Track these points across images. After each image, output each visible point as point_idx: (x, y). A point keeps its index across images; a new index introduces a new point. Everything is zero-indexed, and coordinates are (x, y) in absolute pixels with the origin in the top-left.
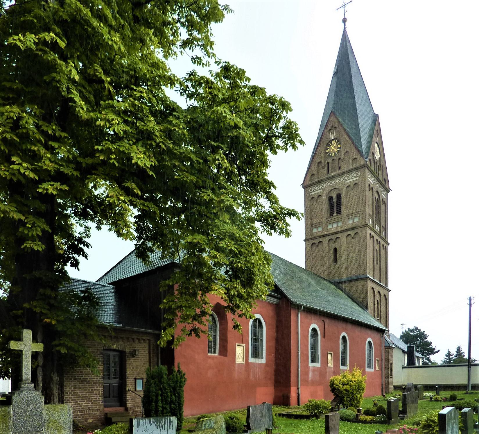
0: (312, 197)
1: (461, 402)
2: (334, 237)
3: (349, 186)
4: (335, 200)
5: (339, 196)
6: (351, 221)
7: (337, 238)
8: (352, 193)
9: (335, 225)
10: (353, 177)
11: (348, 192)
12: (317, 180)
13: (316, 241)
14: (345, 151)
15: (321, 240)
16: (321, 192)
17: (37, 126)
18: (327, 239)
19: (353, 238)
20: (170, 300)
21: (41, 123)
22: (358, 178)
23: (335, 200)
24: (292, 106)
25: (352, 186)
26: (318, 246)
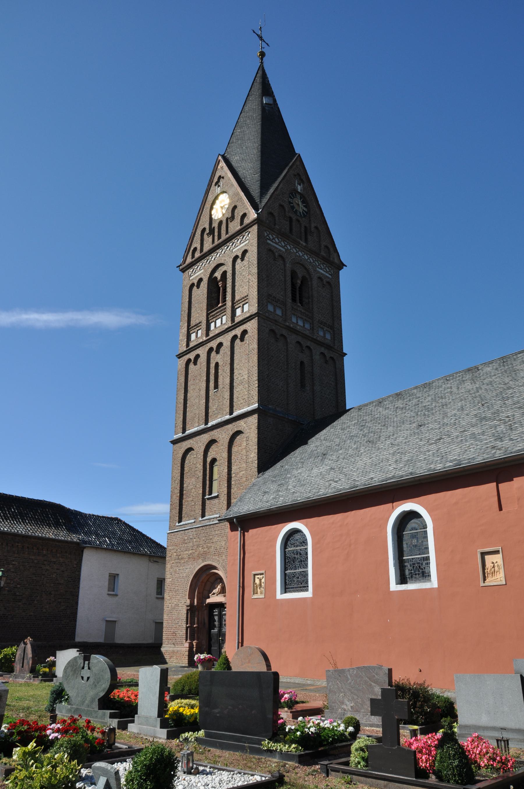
4: (299, 282)
7: (282, 335)
9: (300, 323)
10: (280, 244)
15: (285, 332)
22: (284, 250)
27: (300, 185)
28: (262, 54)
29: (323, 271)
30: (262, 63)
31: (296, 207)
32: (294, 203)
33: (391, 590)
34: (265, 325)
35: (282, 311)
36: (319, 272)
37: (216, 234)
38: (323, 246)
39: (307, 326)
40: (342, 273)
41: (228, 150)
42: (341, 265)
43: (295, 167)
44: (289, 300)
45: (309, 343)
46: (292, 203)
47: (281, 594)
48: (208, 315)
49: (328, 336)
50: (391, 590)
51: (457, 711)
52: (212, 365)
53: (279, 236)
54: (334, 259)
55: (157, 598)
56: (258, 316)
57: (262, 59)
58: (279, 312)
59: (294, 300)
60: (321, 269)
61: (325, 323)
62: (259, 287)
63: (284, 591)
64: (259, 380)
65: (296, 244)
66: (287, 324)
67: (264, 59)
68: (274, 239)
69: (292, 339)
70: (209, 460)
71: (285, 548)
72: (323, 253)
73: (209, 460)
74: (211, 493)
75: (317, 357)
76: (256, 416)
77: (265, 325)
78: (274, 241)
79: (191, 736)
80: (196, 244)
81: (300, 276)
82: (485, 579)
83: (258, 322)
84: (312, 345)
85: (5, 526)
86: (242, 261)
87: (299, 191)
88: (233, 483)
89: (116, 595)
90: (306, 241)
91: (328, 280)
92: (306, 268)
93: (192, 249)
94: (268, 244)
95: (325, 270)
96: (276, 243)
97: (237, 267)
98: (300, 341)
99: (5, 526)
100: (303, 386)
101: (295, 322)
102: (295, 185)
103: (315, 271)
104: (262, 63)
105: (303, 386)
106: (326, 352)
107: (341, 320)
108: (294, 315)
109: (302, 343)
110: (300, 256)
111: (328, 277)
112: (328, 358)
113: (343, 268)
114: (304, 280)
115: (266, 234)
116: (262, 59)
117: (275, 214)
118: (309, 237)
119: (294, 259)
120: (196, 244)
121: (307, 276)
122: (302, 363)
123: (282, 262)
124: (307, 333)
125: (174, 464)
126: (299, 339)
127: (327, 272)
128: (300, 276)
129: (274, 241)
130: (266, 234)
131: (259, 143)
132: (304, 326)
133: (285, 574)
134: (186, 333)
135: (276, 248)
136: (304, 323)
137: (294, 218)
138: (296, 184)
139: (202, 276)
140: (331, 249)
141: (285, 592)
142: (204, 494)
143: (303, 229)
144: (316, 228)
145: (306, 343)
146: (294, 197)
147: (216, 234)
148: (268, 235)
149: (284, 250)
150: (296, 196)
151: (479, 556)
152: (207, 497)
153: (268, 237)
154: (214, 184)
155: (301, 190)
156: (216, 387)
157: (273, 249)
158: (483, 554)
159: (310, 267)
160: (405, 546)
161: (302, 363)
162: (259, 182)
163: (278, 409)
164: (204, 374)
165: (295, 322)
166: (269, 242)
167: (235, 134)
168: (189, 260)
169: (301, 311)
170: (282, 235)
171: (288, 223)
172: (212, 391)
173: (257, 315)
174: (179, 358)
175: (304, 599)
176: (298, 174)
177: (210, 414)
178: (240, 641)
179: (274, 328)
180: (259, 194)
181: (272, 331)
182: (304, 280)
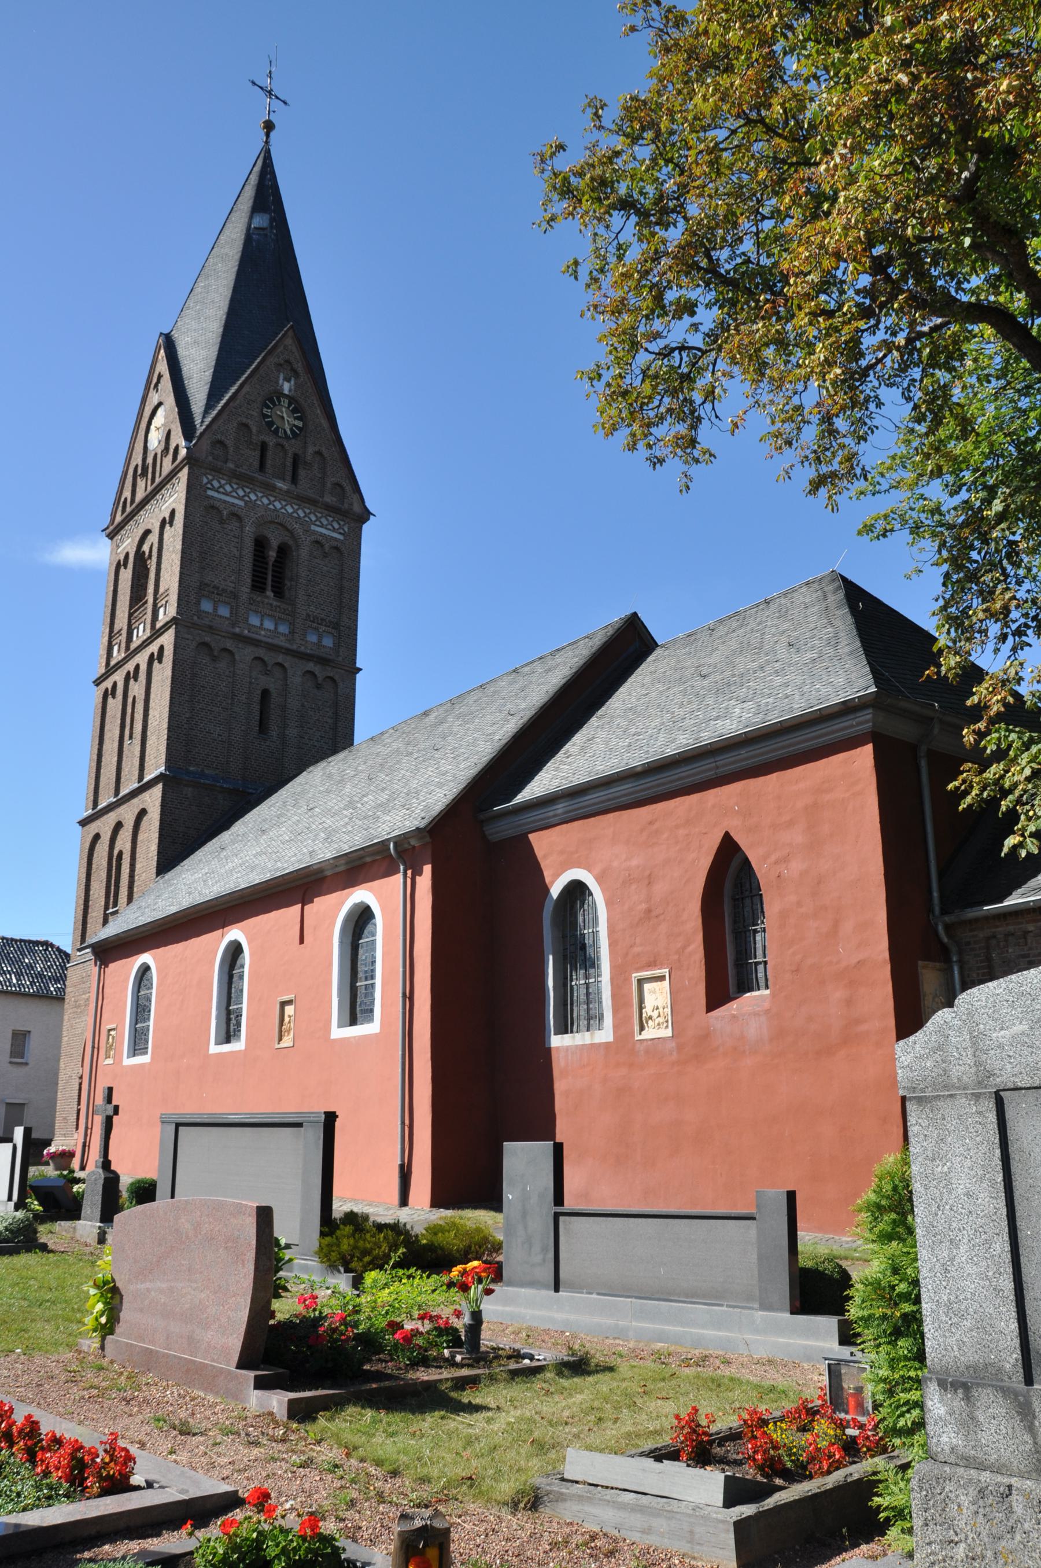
4: (272, 554)
7: (225, 650)
9: (269, 625)
10: (234, 494)
15: (229, 644)
16: (240, 507)
19: (267, 673)
22: (241, 503)
23: (272, 554)
26: (215, 659)
27: (289, 381)
28: (269, 126)
29: (327, 529)
30: (267, 142)
31: (278, 422)
32: (274, 417)
33: (611, 1039)
34: (189, 636)
35: (232, 609)
36: (314, 533)
37: (150, 476)
38: (329, 485)
39: (283, 629)
40: (368, 529)
41: (179, 323)
42: (365, 515)
43: (280, 349)
44: (245, 589)
45: (280, 658)
46: (270, 417)
47: (128, 1057)
48: (130, 615)
49: (328, 642)
50: (611, 1039)
52: (130, 700)
53: (235, 480)
54: (351, 504)
55: (11, 1063)
56: (176, 624)
57: (268, 135)
58: (224, 611)
59: (258, 585)
60: (322, 526)
61: (322, 619)
62: (181, 574)
63: (132, 1053)
64: (169, 729)
65: (269, 489)
66: (237, 630)
67: (272, 134)
68: (221, 486)
69: (245, 654)
70: (116, 852)
71: (139, 992)
72: (328, 499)
73: (116, 852)
74: (115, 904)
75: (296, 679)
76: (160, 786)
77: (189, 636)
78: (221, 490)
79: (305, 1269)
80: (127, 494)
81: (275, 543)
82: (280, 1039)
83: (176, 633)
84: (287, 661)
86: (171, 526)
87: (286, 392)
88: (135, 889)
89: (26, 1064)
90: (294, 480)
91: (335, 544)
92: (287, 530)
93: (122, 500)
95: (330, 527)
96: (226, 494)
97: (166, 536)
98: (262, 656)
100: (263, 726)
101: (258, 624)
102: (277, 383)
103: (307, 531)
104: (267, 142)
105: (263, 726)
106: (317, 669)
107: (357, 611)
108: (256, 612)
109: (266, 659)
110: (276, 510)
111: (336, 539)
112: (320, 680)
113: (368, 519)
114: (283, 551)
115: (205, 480)
116: (268, 135)
117: (227, 442)
118: (302, 473)
119: (262, 516)
120: (127, 494)
121: (291, 542)
122: (265, 694)
123: (237, 524)
124: (281, 642)
125: (81, 858)
126: (261, 652)
127: (334, 530)
128: (275, 543)
129: (221, 490)
130: (205, 480)
131: (226, 309)
132: (276, 628)
133: (136, 1029)
134: (106, 644)
135: (225, 502)
136: (276, 625)
137: (271, 441)
138: (281, 381)
139: (129, 549)
140: (348, 488)
141: (134, 1056)
142: (106, 908)
144: (319, 453)
145: (270, 658)
146: (274, 405)
147: (150, 476)
148: (209, 482)
149: (241, 503)
150: (279, 401)
151: (278, 1006)
152: (111, 910)
153: (209, 486)
154: (152, 386)
155: (290, 390)
156: (131, 737)
158: (641, 982)
159: (297, 526)
160: (233, 990)
161: (265, 694)
162: (208, 386)
163: (206, 771)
164: (119, 715)
165: (258, 624)
166: (210, 493)
167: (196, 291)
168: (119, 518)
169: (271, 605)
170: (240, 478)
171: (257, 453)
172: (127, 742)
173: (174, 621)
174: (97, 685)
175: (142, 1066)
176: (288, 362)
177: (122, 780)
178: (407, 1122)
179: (207, 639)
180: (203, 409)
181: (205, 644)
182: (283, 551)
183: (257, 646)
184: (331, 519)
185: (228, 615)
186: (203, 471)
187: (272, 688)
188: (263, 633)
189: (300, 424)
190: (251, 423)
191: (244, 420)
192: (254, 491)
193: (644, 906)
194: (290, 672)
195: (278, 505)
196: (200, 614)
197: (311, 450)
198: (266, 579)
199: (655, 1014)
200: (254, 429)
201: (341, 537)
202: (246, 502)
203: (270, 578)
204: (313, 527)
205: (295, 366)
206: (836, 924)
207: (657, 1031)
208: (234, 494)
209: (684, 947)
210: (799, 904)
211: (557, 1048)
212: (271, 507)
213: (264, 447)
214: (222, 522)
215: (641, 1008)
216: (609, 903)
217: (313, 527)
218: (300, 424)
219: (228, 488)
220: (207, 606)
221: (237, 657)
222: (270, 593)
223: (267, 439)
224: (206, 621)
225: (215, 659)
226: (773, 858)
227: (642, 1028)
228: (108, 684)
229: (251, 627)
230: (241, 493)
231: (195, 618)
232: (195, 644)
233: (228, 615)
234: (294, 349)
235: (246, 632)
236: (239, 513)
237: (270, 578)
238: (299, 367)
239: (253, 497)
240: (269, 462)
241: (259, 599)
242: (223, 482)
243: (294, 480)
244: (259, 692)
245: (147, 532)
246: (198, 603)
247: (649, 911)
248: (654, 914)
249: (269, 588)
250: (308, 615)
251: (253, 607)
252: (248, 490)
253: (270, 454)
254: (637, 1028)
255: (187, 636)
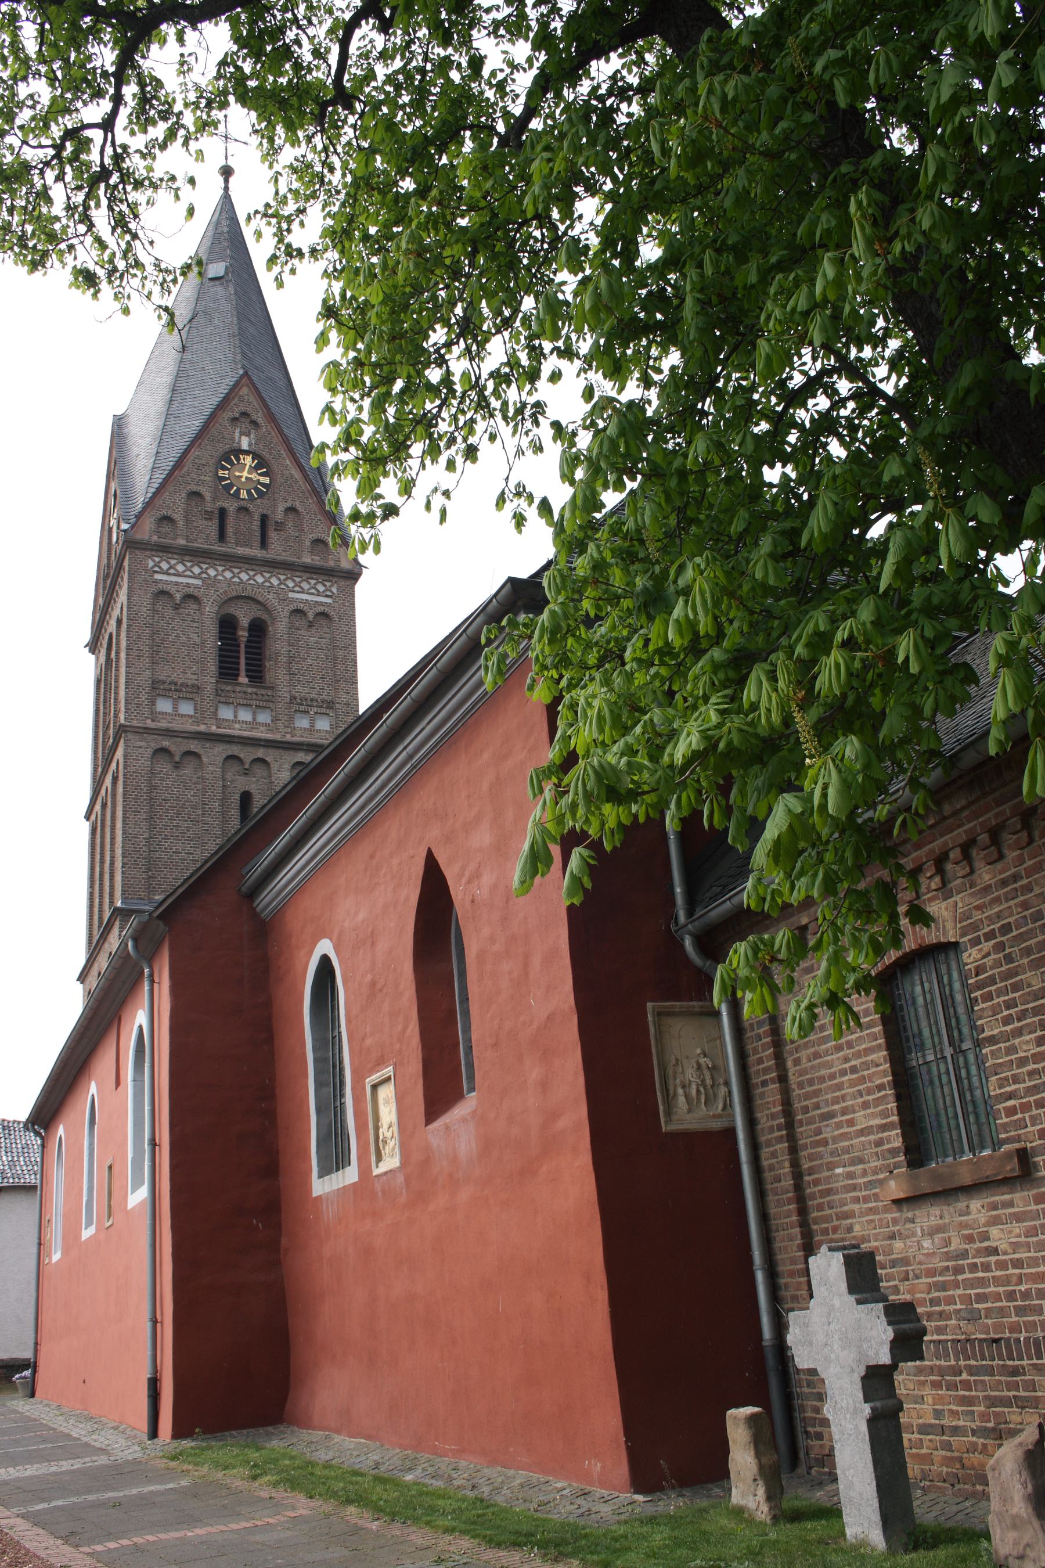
0: (160, 586)
1: (599, 1516)
2: (247, 754)
3: (298, 611)
4: (243, 634)
5: (258, 629)
6: (303, 723)
7: (189, 753)
8: (310, 638)
9: (245, 715)
10: (188, 573)
11: (292, 627)
12: (182, 542)
13: (177, 747)
14: (289, 505)
15: (194, 746)
16: (196, 587)
17: (768, 357)
18: (220, 751)
19: (246, 773)
20: (946, 813)
21: (774, 357)
22: (199, 582)
23: (243, 634)
24: (38, 274)
25: (311, 616)
26: (177, 766)
27: (248, 435)
30: (226, 188)
36: (293, 600)
38: (308, 543)
40: (361, 588)
44: (210, 679)
45: (260, 753)
51: (821, 1397)
53: (187, 558)
57: (226, 181)
59: (227, 671)
67: (231, 180)
77: (143, 744)
81: (244, 621)
84: (270, 755)
85: (11, 1473)
90: (264, 543)
91: (320, 609)
92: (258, 602)
94: (156, 582)
96: (178, 575)
98: (236, 753)
99: (11, 1473)
102: (233, 439)
104: (226, 188)
109: (242, 756)
110: (242, 582)
111: (322, 604)
115: (151, 564)
116: (226, 181)
117: (175, 516)
118: (273, 535)
121: (265, 617)
123: (196, 607)
126: (235, 750)
127: (318, 594)
128: (244, 621)
129: (172, 571)
135: (177, 584)
137: (231, 506)
143: (256, 525)
144: (292, 510)
149: (199, 582)
155: (250, 445)
157: (168, 588)
166: (157, 577)
171: (215, 523)
181: (163, 751)
183: (229, 742)
184: (313, 582)
185: (192, 713)
186: (148, 553)
187: (253, 789)
188: (237, 726)
189: (266, 480)
190: (202, 489)
191: (195, 488)
192: (214, 567)
193: (369, 977)
194: (274, 766)
195: (244, 576)
196: (154, 716)
197: (281, 508)
198: (238, 663)
199: (389, 1135)
200: (208, 496)
201: (329, 600)
202: (203, 580)
203: (243, 661)
204: (291, 595)
205: (254, 417)
206: (526, 965)
207: (391, 1162)
208: (188, 573)
209: (404, 1030)
210: (492, 940)
211: (319, 1198)
212: (236, 580)
213: (223, 513)
214: (177, 607)
215: (377, 1128)
216: (345, 982)
217: (291, 595)
218: (266, 480)
219: (180, 568)
220: (164, 706)
221: (205, 759)
222: (243, 679)
223: (225, 505)
224: (164, 724)
225: (177, 766)
226: (467, 874)
227: (379, 1158)
228: (93, 817)
229: (219, 723)
230: (197, 570)
231: (149, 721)
232: (150, 751)
233: (192, 713)
234: (252, 398)
235: (214, 728)
236: (196, 594)
237: (243, 661)
238: (259, 418)
239: (212, 572)
240: (230, 530)
241: (229, 688)
242: (173, 562)
243: (264, 543)
244: (237, 796)
245: (111, 635)
246: (153, 703)
247: (373, 984)
248: (379, 986)
249: (243, 672)
250: (293, 698)
251: (223, 699)
252: (204, 566)
253: (230, 520)
254: (373, 1158)
255: (138, 744)
